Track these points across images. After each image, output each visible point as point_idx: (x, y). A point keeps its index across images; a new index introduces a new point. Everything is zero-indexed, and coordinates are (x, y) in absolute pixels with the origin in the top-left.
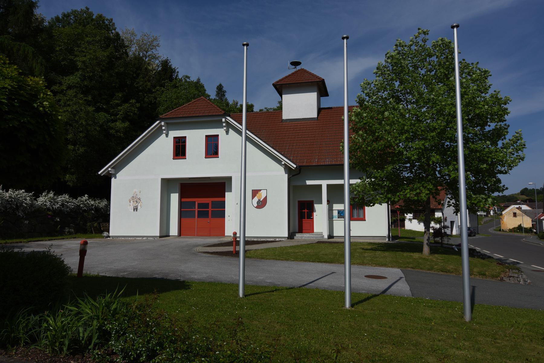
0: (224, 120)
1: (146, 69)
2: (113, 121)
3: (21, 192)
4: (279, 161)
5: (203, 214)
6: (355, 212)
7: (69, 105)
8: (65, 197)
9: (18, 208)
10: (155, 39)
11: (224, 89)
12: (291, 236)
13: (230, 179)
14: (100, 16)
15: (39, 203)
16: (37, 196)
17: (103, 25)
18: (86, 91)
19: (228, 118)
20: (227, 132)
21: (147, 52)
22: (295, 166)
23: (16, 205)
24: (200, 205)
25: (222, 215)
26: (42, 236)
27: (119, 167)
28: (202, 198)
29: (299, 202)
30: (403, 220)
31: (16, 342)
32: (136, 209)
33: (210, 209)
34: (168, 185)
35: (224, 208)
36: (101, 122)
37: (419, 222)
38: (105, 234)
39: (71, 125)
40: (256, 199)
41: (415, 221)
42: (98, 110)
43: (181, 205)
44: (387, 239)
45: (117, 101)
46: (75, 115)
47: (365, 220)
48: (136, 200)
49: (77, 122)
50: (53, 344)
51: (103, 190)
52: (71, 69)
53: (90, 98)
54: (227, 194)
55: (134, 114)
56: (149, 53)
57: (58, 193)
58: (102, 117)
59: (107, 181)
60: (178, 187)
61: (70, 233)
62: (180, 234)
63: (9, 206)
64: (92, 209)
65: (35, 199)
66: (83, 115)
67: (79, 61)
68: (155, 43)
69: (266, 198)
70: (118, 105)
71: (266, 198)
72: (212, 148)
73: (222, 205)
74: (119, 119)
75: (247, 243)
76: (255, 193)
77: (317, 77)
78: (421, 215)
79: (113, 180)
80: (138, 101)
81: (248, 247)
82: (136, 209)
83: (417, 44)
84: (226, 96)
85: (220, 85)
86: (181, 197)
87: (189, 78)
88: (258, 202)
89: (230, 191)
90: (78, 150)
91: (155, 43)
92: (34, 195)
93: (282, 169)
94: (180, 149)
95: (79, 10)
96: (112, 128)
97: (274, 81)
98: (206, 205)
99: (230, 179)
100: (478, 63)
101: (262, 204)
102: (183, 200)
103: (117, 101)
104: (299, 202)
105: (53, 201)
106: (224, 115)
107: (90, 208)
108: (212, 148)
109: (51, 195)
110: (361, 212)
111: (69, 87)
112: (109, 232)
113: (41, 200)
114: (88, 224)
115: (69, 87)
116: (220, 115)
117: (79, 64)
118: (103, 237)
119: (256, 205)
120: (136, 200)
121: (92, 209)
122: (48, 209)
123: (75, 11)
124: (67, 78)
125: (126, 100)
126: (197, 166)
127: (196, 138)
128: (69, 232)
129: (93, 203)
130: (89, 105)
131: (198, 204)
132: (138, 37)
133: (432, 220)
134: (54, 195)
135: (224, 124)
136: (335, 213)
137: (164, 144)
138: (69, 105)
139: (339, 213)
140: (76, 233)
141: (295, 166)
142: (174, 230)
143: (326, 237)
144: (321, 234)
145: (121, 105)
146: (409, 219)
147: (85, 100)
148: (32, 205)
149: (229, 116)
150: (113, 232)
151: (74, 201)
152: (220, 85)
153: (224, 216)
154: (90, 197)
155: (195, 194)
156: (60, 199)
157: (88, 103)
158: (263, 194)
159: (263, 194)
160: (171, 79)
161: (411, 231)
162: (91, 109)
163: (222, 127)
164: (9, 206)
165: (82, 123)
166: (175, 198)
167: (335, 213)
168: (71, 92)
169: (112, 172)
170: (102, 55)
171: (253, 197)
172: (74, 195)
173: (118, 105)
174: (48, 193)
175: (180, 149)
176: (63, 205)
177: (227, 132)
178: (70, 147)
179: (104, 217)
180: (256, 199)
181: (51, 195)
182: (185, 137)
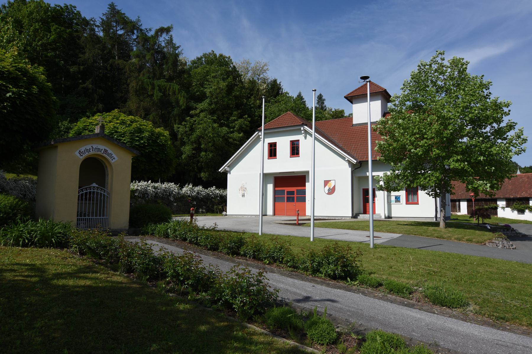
0: (302, 128)
1: (258, 89)
2: (233, 132)
3: (172, 184)
4: (343, 158)
5: (290, 199)
6: (410, 197)
7: (201, 124)
8: (200, 188)
9: (170, 195)
10: (265, 65)
11: (323, 98)
12: (355, 216)
13: (308, 172)
14: (221, 55)
15: (183, 192)
16: (182, 187)
17: (222, 62)
18: (212, 112)
19: (305, 127)
20: (306, 138)
21: (259, 76)
22: (356, 161)
23: (167, 194)
24: (288, 193)
25: (303, 199)
26: (185, 214)
27: (232, 166)
28: (289, 186)
29: (363, 189)
30: (496, 208)
31: (147, 233)
32: (243, 196)
33: (295, 196)
34: (266, 177)
35: (305, 194)
36: (222, 135)
37: (513, 209)
38: (224, 213)
39: (203, 138)
40: (327, 188)
41: (508, 210)
42: (221, 125)
43: (275, 192)
44: (435, 219)
45: (234, 118)
46: (205, 130)
47: (418, 204)
48: (244, 189)
49: (207, 135)
50: (159, 233)
51: (222, 183)
52: (201, 98)
53: (215, 118)
54: (307, 184)
55: (247, 126)
56: (261, 76)
57: (195, 185)
58: (225, 129)
59: (225, 175)
60: (272, 180)
61: (203, 212)
62: (274, 214)
63: (165, 194)
64: (218, 197)
65: (181, 189)
66: (210, 129)
67: (208, 91)
68: (265, 68)
69: (334, 186)
70: (235, 120)
71: (334, 186)
72: (295, 150)
73: (304, 192)
74: (236, 131)
75: (315, 220)
76: (326, 183)
77: (381, 88)
78: (515, 203)
79: (228, 175)
80: (249, 117)
81: (315, 221)
82: (243, 196)
83: (436, 62)
84: (325, 104)
85: (320, 95)
86: (275, 186)
87: (288, 94)
88: (329, 190)
89: (309, 182)
90: (209, 155)
91: (265, 68)
92: (179, 187)
93: (347, 164)
94: (272, 151)
95: (208, 53)
96: (231, 138)
97: (345, 95)
98: (292, 193)
99: (308, 172)
100: (483, 76)
101: (331, 191)
102: (277, 189)
103: (234, 118)
104: (363, 189)
105: (192, 190)
106: (303, 125)
107: (216, 196)
108: (295, 150)
109: (191, 186)
110: (416, 197)
111: (202, 111)
112: (226, 211)
113: (185, 189)
114: (215, 207)
115: (202, 111)
116: (299, 125)
117: (208, 94)
118: (223, 215)
119: (327, 192)
120: (244, 189)
121: (218, 197)
122: (189, 196)
123: (206, 54)
124: (200, 104)
125: (241, 116)
126: (285, 164)
127: (283, 143)
128: (202, 212)
129: (217, 192)
130: (215, 123)
131: (287, 192)
132: (252, 65)
133: (527, 209)
134: (193, 186)
135: (303, 132)
136: (393, 199)
137: (259, 150)
138: (201, 124)
139: (396, 198)
140: (207, 213)
141: (356, 161)
142: (270, 211)
143: (383, 217)
144: (379, 215)
145: (237, 120)
146: (502, 207)
147: (212, 119)
148: (179, 193)
149: (306, 125)
150: (229, 212)
151: (206, 190)
152: (320, 95)
153: (305, 201)
154: (216, 188)
155: (293, 186)
156: (196, 189)
157: (215, 121)
158: (332, 184)
159: (332, 184)
160: (278, 94)
161: (504, 219)
162: (215, 125)
163: (301, 134)
164: (165, 194)
165: (210, 136)
166: (270, 187)
167: (393, 199)
168: (202, 115)
169: (228, 169)
170: (223, 84)
171: (325, 186)
172: (206, 187)
173: (235, 120)
174: (189, 185)
175: (272, 151)
176: (198, 193)
177: (306, 138)
178: (203, 153)
179: (223, 201)
180: (327, 188)
181: (191, 186)
182: (299, 140)
